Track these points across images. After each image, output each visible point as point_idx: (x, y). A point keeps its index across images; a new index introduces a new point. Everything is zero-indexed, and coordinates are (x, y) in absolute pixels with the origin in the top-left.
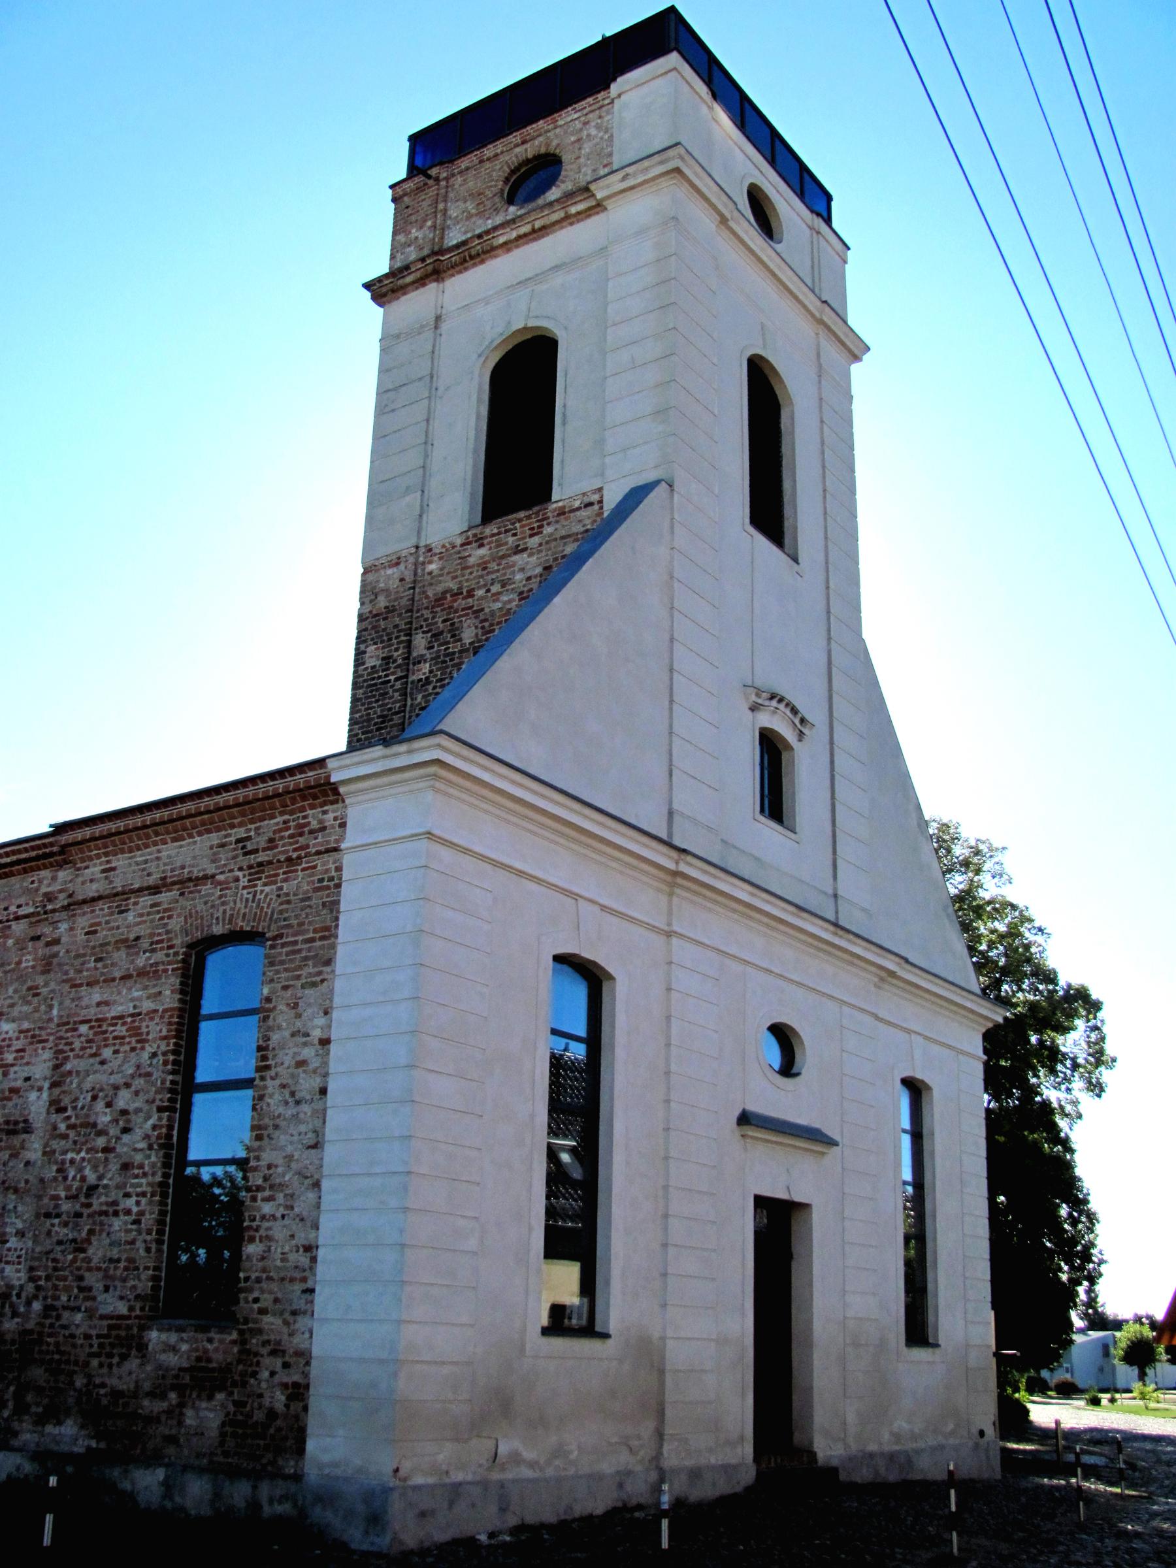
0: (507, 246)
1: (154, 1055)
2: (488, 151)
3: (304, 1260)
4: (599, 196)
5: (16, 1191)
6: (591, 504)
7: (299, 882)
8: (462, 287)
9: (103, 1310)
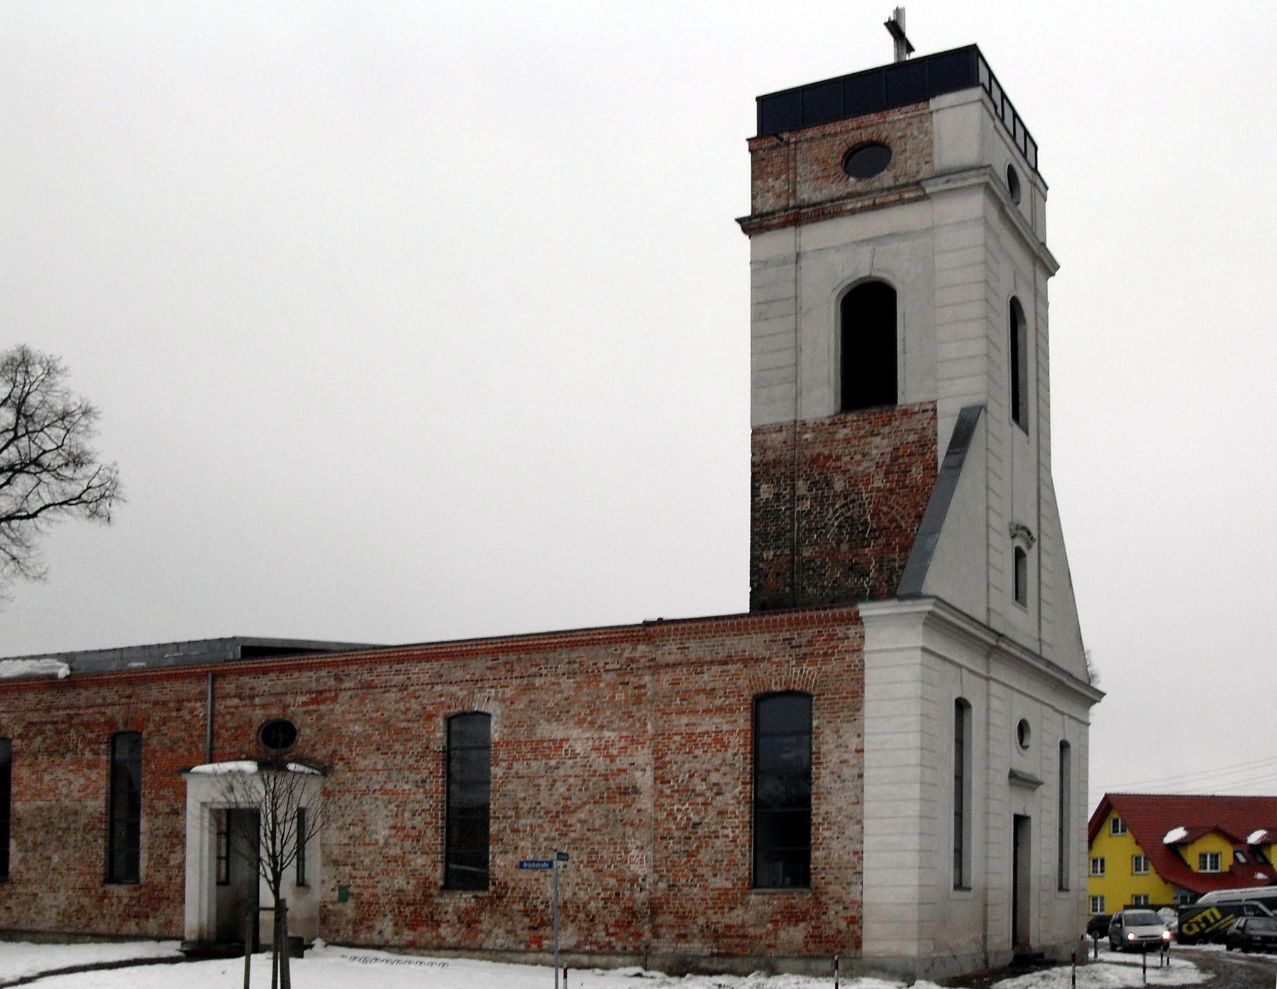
0: (853, 212)
1: (735, 754)
2: (830, 128)
3: (855, 859)
4: (928, 191)
5: (632, 825)
6: (926, 411)
7: (833, 666)
8: (815, 235)
9: (712, 886)
